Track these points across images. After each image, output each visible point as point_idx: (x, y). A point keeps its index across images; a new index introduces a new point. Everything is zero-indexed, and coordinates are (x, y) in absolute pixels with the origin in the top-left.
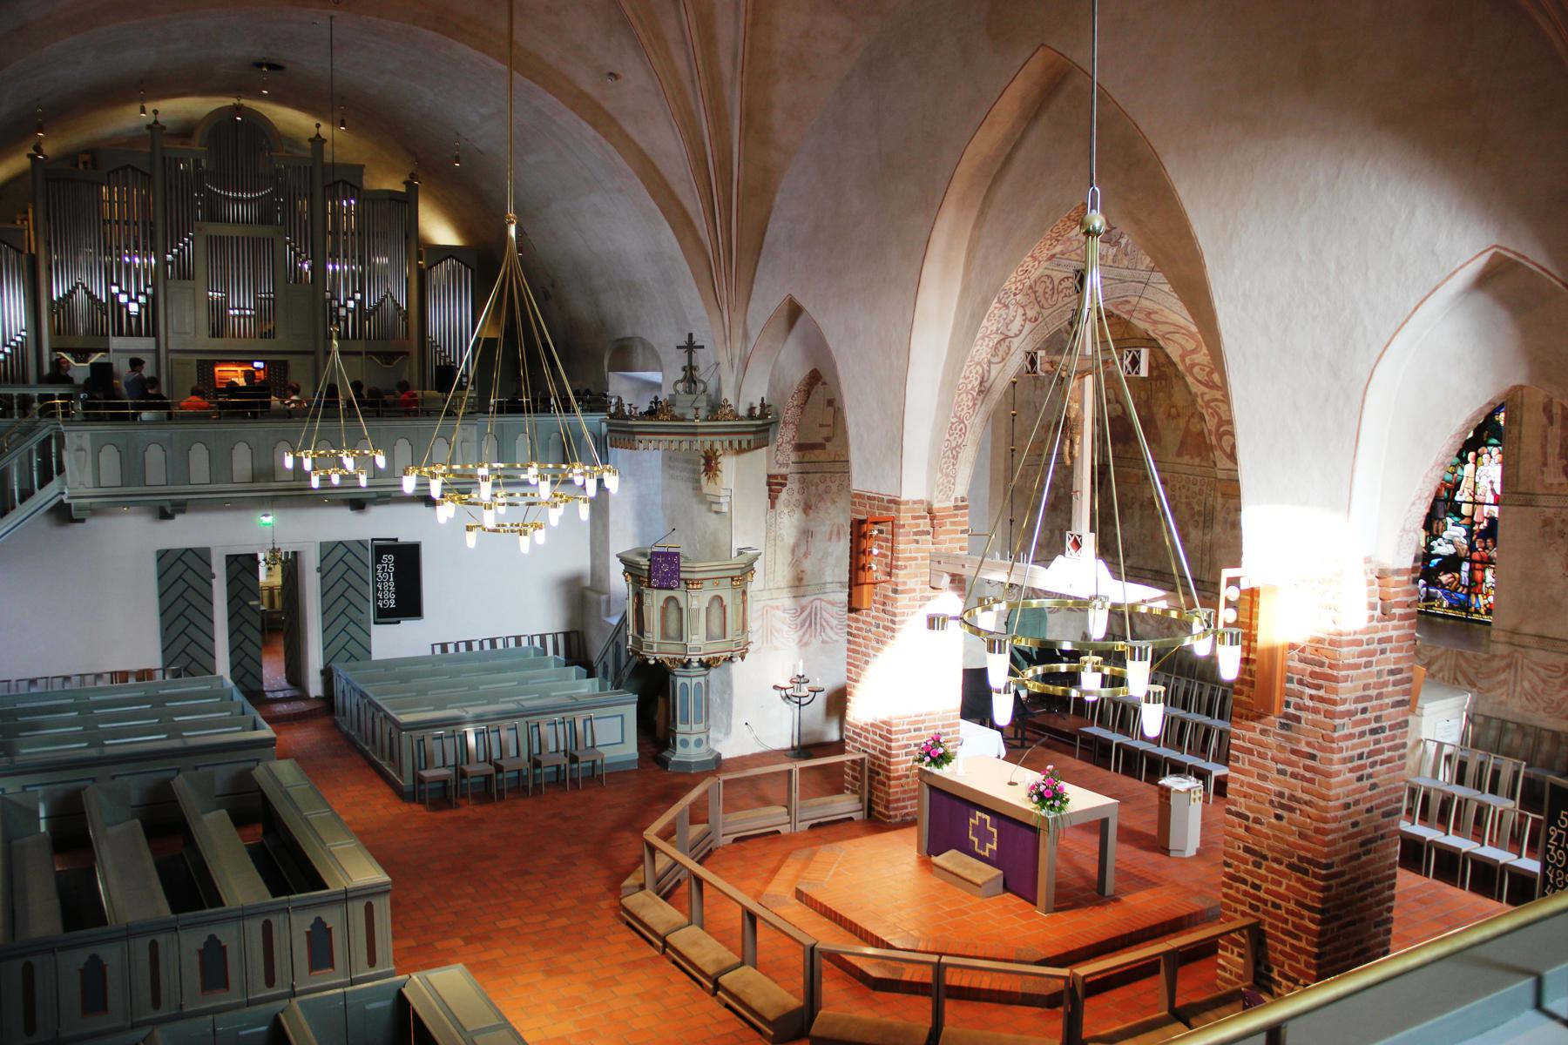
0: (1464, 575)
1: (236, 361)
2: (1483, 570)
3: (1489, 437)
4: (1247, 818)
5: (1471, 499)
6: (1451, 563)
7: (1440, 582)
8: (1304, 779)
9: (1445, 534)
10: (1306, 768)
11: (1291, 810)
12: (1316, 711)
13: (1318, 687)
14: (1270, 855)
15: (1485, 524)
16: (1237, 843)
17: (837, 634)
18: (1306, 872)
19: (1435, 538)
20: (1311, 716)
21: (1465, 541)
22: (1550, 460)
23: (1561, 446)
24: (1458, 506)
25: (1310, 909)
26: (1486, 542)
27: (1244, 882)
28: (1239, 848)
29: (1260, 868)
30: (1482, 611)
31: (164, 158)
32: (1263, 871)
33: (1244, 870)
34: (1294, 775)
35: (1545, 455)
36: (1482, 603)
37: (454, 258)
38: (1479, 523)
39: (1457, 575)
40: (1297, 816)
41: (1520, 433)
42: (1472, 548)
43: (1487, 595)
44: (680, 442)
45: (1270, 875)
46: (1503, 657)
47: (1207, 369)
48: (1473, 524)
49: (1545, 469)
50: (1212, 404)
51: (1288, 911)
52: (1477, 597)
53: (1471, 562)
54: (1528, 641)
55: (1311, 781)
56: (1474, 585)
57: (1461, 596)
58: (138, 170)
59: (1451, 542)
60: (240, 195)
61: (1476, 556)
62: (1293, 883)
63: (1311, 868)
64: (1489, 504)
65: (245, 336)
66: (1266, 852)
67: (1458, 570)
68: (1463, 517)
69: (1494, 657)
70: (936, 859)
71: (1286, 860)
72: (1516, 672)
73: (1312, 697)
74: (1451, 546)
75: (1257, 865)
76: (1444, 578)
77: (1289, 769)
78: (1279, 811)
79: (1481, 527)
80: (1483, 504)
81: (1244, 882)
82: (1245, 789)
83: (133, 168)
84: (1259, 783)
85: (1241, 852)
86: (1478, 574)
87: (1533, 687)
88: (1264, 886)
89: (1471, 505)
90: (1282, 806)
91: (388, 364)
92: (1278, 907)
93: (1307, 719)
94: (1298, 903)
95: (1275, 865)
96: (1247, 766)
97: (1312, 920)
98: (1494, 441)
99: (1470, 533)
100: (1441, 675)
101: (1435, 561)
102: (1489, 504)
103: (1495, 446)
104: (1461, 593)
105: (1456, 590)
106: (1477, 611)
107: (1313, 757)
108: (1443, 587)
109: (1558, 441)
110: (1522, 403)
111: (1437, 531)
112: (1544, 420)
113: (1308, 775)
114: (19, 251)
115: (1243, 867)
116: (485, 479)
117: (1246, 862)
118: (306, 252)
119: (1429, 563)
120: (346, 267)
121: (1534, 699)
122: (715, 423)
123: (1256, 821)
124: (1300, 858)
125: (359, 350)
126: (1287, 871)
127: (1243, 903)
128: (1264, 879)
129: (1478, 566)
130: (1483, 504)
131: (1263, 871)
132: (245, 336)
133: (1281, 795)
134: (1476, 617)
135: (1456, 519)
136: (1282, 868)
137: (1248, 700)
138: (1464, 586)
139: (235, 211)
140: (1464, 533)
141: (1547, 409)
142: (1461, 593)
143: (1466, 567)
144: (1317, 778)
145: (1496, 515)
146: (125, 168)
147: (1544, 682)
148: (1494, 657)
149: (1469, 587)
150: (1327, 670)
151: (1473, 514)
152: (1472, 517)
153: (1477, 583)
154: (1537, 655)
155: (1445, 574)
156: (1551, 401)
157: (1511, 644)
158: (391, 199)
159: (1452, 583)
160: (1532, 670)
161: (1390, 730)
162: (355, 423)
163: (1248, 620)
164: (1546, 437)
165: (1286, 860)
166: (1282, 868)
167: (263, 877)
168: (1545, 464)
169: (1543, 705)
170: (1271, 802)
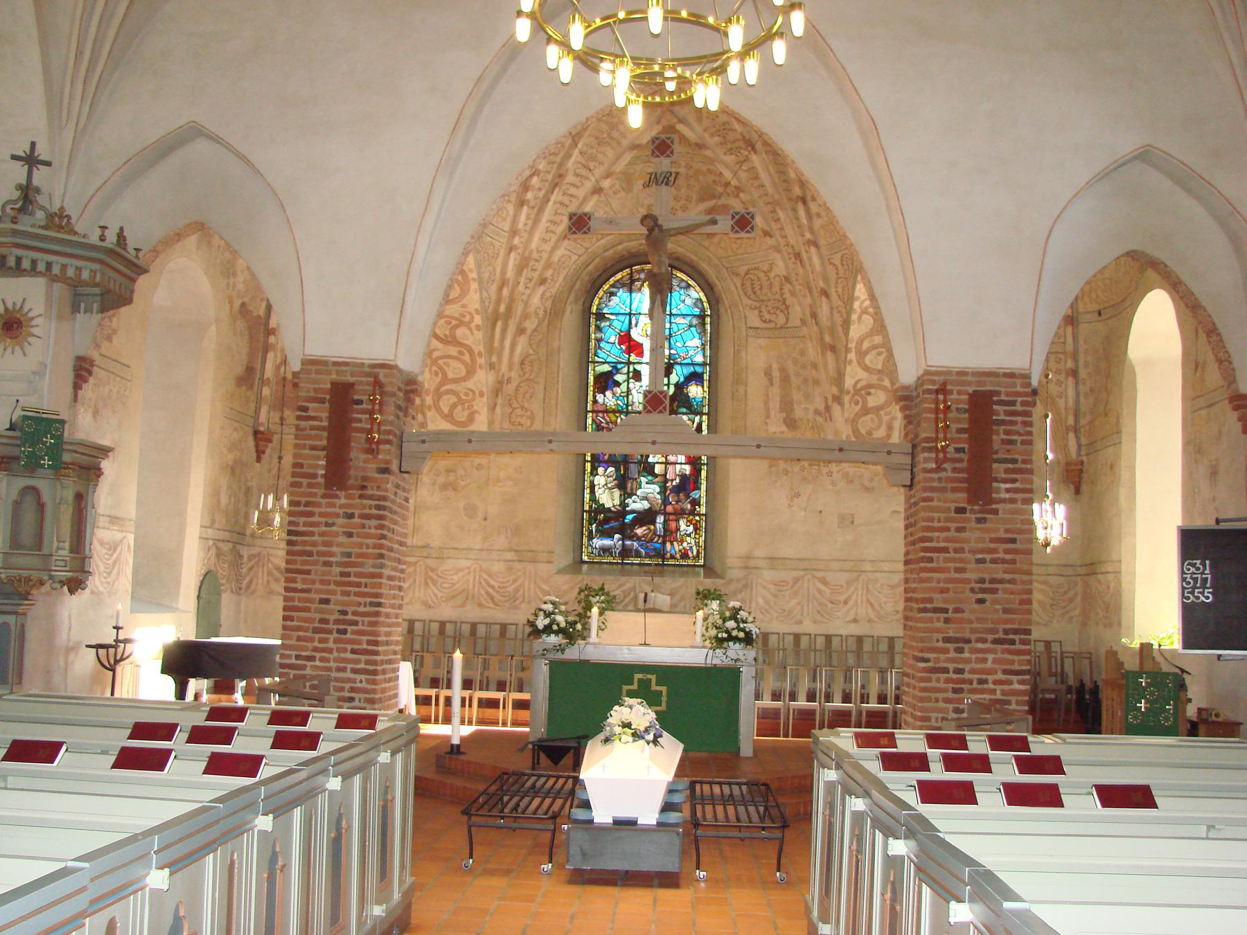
0: (659, 526)
2: (677, 521)
3: (678, 407)
4: (946, 611)
5: (664, 460)
6: (646, 517)
7: (636, 534)
8: (1004, 561)
9: (639, 492)
10: (1007, 552)
11: (994, 591)
12: (1013, 501)
13: (1013, 481)
14: (973, 637)
15: (678, 481)
16: (936, 636)
17: (102, 583)
18: (1013, 642)
19: (630, 496)
20: (1008, 506)
21: (659, 497)
22: (772, 413)
23: (781, 402)
24: (652, 466)
25: (1017, 673)
26: (678, 496)
27: (946, 670)
28: (938, 641)
29: (963, 652)
30: (678, 556)
32: (966, 655)
33: (943, 660)
34: (994, 561)
35: (768, 410)
36: (677, 549)
38: (672, 480)
39: (652, 527)
40: (1000, 595)
41: (746, 392)
42: (665, 502)
43: (682, 542)
45: (974, 656)
46: (738, 580)
47: (454, 322)
48: (666, 481)
49: (768, 421)
50: (441, 362)
51: (995, 682)
52: (672, 544)
53: (665, 514)
54: (761, 563)
55: (1013, 562)
56: (670, 534)
57: (657, 545)
59: (646, 498)
61: (669, 509)
62: (999, 655)
63: (1016, 637)
64: (681, 464)
66: (967, 635)
67: (653, 522)
68: (656, 476)
69: (731, 581)
70: (542, 755)
71: (990, 637)
72: (752, 590)
73: (1008, 490)
74: (645, 503)
75: (959, 650)
76: (639, 531)
77: (988, 557)
78: (980, 596)
79: (674, 483)
80: (675, 463)
81: (946, 670)
82: (941, 585)
84: (957, 575)
85: (940, 644)
86: (673, 525)
87: (767, 602)
88: (967, 667)
89: (663, 466)
90: (984, 591)
92: (985, 681)
93: (1004, 509)
94: (1005, 672)
95: (980, 645)
96: (942, 564)
97: (1020, 682)
98: (684, 410)
99: (663, 489)
100: (682, 604)
101: (630, 517)
102: (681, 464)
103: (684, 414)
104: (657, 542)
105: (651, 540)
106: (672, 557)
107: (1013, 541)
108: (639, 539)
109: (778, 399)
110: (747, 368)
111: (632, 489)
112: (765, 382)
113: (1008, 557)
115: (942, 656)
116: (684, 83)
117: (946, 651)
119: (624, 518)
121: (767, 611)
123: (957, 610)
124: (1006, 632)
126: (993, 646)
127: (945, 690)
128: (968, 661)
129: (671, 517)
130: (675, 463)
131: (966, 655)
133: (982, 581)
134: (671, 562)
135: (650, 478)
136: (987, 645)
137: (939, 504)
138: (659, 536)
140: (658, 489)
141: (768, 373)
142: (657, 542)
143: (660, 519)
144: (1018, 557)
145: (688, 473)
147: (775, 596)
148: (731, 581)
149: (664, 536)
150: (1019, 465)
151: (666, 473)
152: (665, 475)
153: (672, 532)
154: (767, 574)
155: (641, 527)
156: (771, 366)
157: (747, 568)
159: (647, 534)
160: (764, 587)
161: (963, 549)
163: (934, 435)
164: (768, 395)
165: (990, 637)
166: (987, 645)
167: (148, 723)
168: (768, 417)
169: (775, 615)
170: (972, 590)
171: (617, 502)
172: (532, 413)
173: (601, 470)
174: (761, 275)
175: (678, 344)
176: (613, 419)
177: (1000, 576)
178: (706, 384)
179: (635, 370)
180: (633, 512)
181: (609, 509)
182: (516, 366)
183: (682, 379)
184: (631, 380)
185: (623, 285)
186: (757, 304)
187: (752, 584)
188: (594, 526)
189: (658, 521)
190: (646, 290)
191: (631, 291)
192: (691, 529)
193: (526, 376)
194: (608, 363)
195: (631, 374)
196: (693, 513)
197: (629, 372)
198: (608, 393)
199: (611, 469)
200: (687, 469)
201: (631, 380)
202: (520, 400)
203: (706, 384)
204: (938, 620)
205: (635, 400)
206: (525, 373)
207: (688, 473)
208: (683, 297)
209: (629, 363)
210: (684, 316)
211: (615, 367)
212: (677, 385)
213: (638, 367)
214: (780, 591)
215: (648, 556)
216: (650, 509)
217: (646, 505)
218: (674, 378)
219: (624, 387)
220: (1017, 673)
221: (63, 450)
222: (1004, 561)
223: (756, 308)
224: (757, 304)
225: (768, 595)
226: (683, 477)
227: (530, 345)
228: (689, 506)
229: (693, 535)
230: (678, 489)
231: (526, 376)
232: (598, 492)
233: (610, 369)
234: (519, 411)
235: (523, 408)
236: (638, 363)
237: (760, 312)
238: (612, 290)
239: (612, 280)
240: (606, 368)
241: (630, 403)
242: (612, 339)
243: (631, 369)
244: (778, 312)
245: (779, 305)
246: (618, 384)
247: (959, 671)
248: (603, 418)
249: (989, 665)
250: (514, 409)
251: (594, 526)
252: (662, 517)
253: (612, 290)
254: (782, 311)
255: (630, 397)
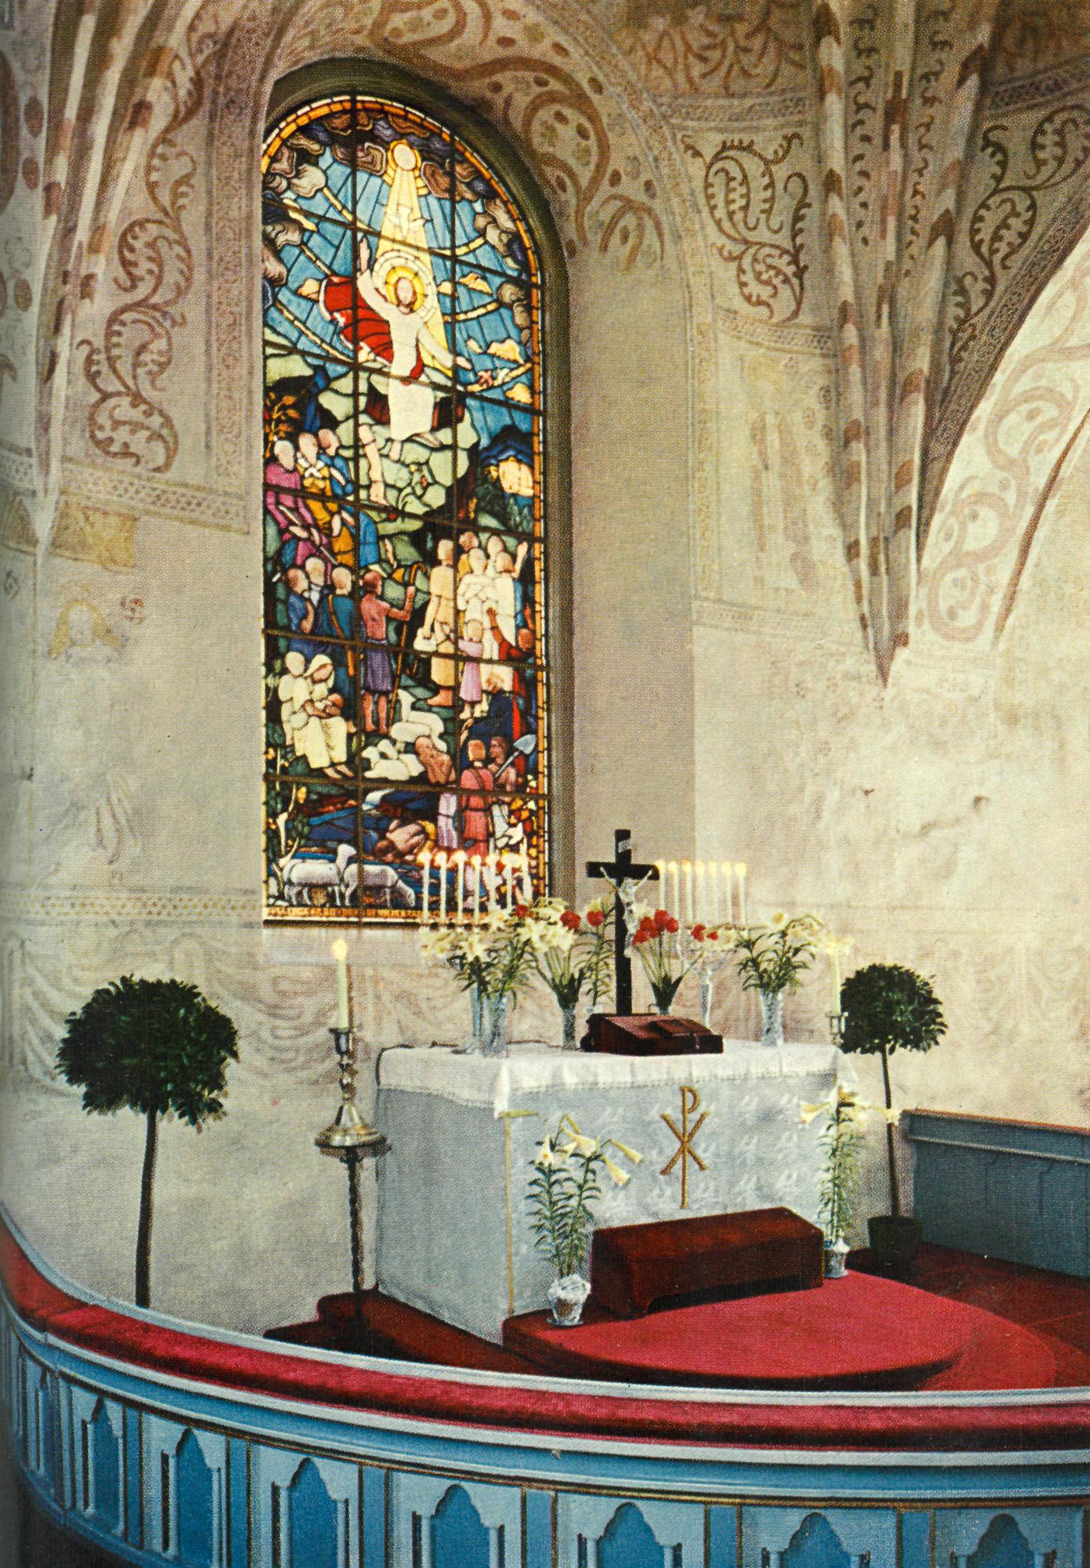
9: (395, 731)
19: (376, 735)
38: (473, 704)
39: (430, 827)
42: (459, 759)
48: (458, 705)
59: (411, 748)
64: (490, 661)
68: (436, 689)
74: (410, 758)
89: (451, 663)
98: (487, 521)
101: (375, 797)
102: (490, 661)
111: (376, 722)
135: (420, 692)
140: (438, 726)
143: (448, 804)
145: (507, 686)
152: (455, 689)
155: (404, 823)
171: (341, 755)
172: (168, 421)
173: (294, 660)
174: (753, 166)
175: (473, 344)
176: (322, 516)
178: (538, 461)
179: (372, 391)
180: (383, 782)
181: (320, 772)
182: (111, 240)
183: (485, 442)
184: (363, 418)
185: (333, 140)
186: (737, 249)
188: (282, 819)
189: (443, 809)
190: (404, 155)
191: (354, 165)
192: (518, 833)
193: (142, 291)
194: (304, 354)
195: (363, 401)
196: (520, 789)
197: (355, 395)
198: (306, 442)
199: (321, 659)
200: (505, 677)
201: (363, 418)
202: (124, 367)
203: (538, 461)
205: (376, 475)
206: (134, 281)
207: (507, 686)
208: (481, 222)
209: (355, 367)
210: (484, 272)
211: (319, 370)
212: (473, 451)
213: (377, 381)
216: (422, 778)
217: (410, 767)
218: (466, 435)
219: (345, 431)
221: (152, 1106)
223: (731, 258)
224: (737, 249)
226: (496, 695)
227: (152, 187)
228: (512, 774)
229: (523, 847)
230: (481, 729)
231: (142, 291)
232: (291, 720)
233: (308, 372)
234: (124, 408)
235: (137, 399)
236: (380, 372)
237: (741, 270)
238: (303, 142)
239: (304, 115)
240: (296, 367)
241: (364, 481)
242: (311, 287)
243: (363, 387)
244: (777, 281)
245: (783, 262)
246: (330, 422)
248: (295, 510)
250: (106, 396)
251: (282, 819)
252: (453, 800)
253: (303, 142)
254: (786, 281)
255: (363, 463)
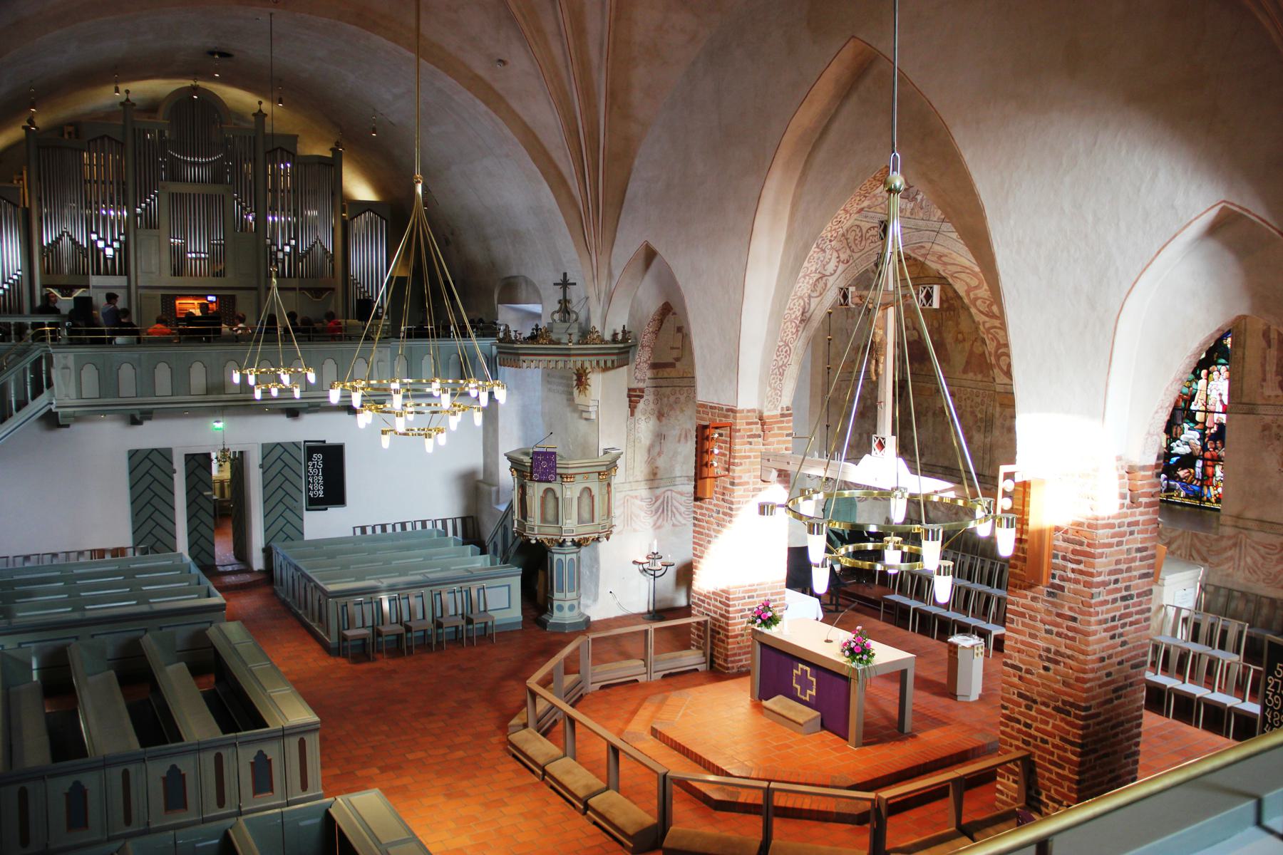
0: (1198, 470)
1: (193, 295)
2: (1214, 467)
3: (1219, 357)
4: (1020, 669)
5: (1203, 408)
7: (1179, 476)
8: (1067, 637)
9: (1182, 437)
10: (1069, 628)
12: (1077, 582)
13: (1079, 562)
14: (1039, 699)
15: (1215, 428)
16: (1012, 690)
17: (685, 518)
18: (1068, 714)
19: (1174, 440)
20: (1072, 586)
21: (1198, 443)
22: (1268, 377)
23: (1277, 365)
25: (1072, 744)
26: (1216, 443)
27: (1018, 721)
28: (1014, 694)
29: (1031, 710)
30: (1213, 500)
31: (134, 130)
32: (1033, 713)
33: (1018, 711)
34: (1059, 634)
35: (1264, 372)
36: (1212, 494)
37: (371, 211)
38: (1211, 428)
39: (1192, 471)
40: (1061, 667)
41: (1244, 354)
42: (1204, 448)
44: (557, 362)
45: (1039, 716)
46: (1230, 538)
47: (988, 302)
49: (1264, 384)
50: (992, 331)
52: (1208, 489)
53: (1204, 459)
54: (1250, 524)
55: (1073, 639)
57: (1196, 488)
58: (113, 139)
59: (1187, 443)
60: (196, 159)
61: (1207, 455)
62: (1058, 722)
63: (1072, 710)
64: (1219, 413)
65: (200, 275)
66: (1035, 697)
67: (1193, 467)
68: (1197, 423)
69: (1222, 537)
71: (1052, 704)
73: (1073, 571)
74: (1187, 447)
76: (1182, 473)
77: (1055, 630)
78: (1046, 664)
79: (1212, 431)
80: (1214, 412)
81: (1018, 721)
82: (1019, 645)
83: (109, 138)
84: (1030, 640)
85: (1015, 697)
86: (1210, 470)
87: (1255, 562)
88: (1034, 725)
89: (1204, 414)
90: (1049, 660)
91: (317, 298)
92: (1046, 742)
93: (1069, 588)
94: (1062, 739)
95: (1043, 708)
96: (1020, 627)
97: (1074, 753)
98: (1223, 361)
99: (1203, 436)
100: (1179, 552)
101: (1174, 459)
102: (1219, 413)
103: (1223, 365)
104: (1195, 485)
105: (1191, 483)
106: (1208, 500)
107: (1074, 619)
108: (1181, 480)
109: (1275, 361)
110: (1245, 330)
111: (1176, 435)
112: (1264, 344)
113: (1070, 634)
114: (16, 206)
115: (1017, 709)
118: (251, 206)
119: (1170, 460)
120: (283, 219)
121: (1255, 572)
122: (585, 346)
123: (1028, 671)
124: (1064, 702)
125: (293, 286)
126: (1053, 712)
127: (1017, 739)
129: (1209, 463)
130: (1214, 412)
131: (1033, 713)
132: (200, 275)
133: (1048, 650)
134: (1207, 505)
135: (1192, 425)
136: (1049, 710)
137: (1021, 572)
138: (1198, 480)
139: (192, 172)
140: (1198, 436)
141: (1266, 334)
142: (1195, 485)
143: (1199, 464)
144: (1078, 636)
145: (1224, 422)
146: (102, 138)
147: (1263, 558)
148: (1222, 537)
149: (1202, 480)
150: (1085, 548)
151: (1206, 420)
152: (1204, 423)
153: (1208, 477)
154: (1257, 536)
155: (1182, 469)
156: (1269, 328)
157: (1236, 527)
158: (320, 163)
159: (1188, 477)
160: (1254, 548)
161: (1137, 597)
162: (290, 346)
163: (1021, 508)
164: (1265, 358)
165: (1052, 704)
166: (1049, 710)
167: (215, 717)
168: (1264, 380)
169: (1262, 577)
177: (1063, 649)
187: (1241, 542)
204: (1015, 676)
214: (1269, 554)
215: (1187, 497)
220: (1072, 744)
222: (1067, 637)
225: (1257, 556)
247: (1028, 726)
249: (1049, 728)
